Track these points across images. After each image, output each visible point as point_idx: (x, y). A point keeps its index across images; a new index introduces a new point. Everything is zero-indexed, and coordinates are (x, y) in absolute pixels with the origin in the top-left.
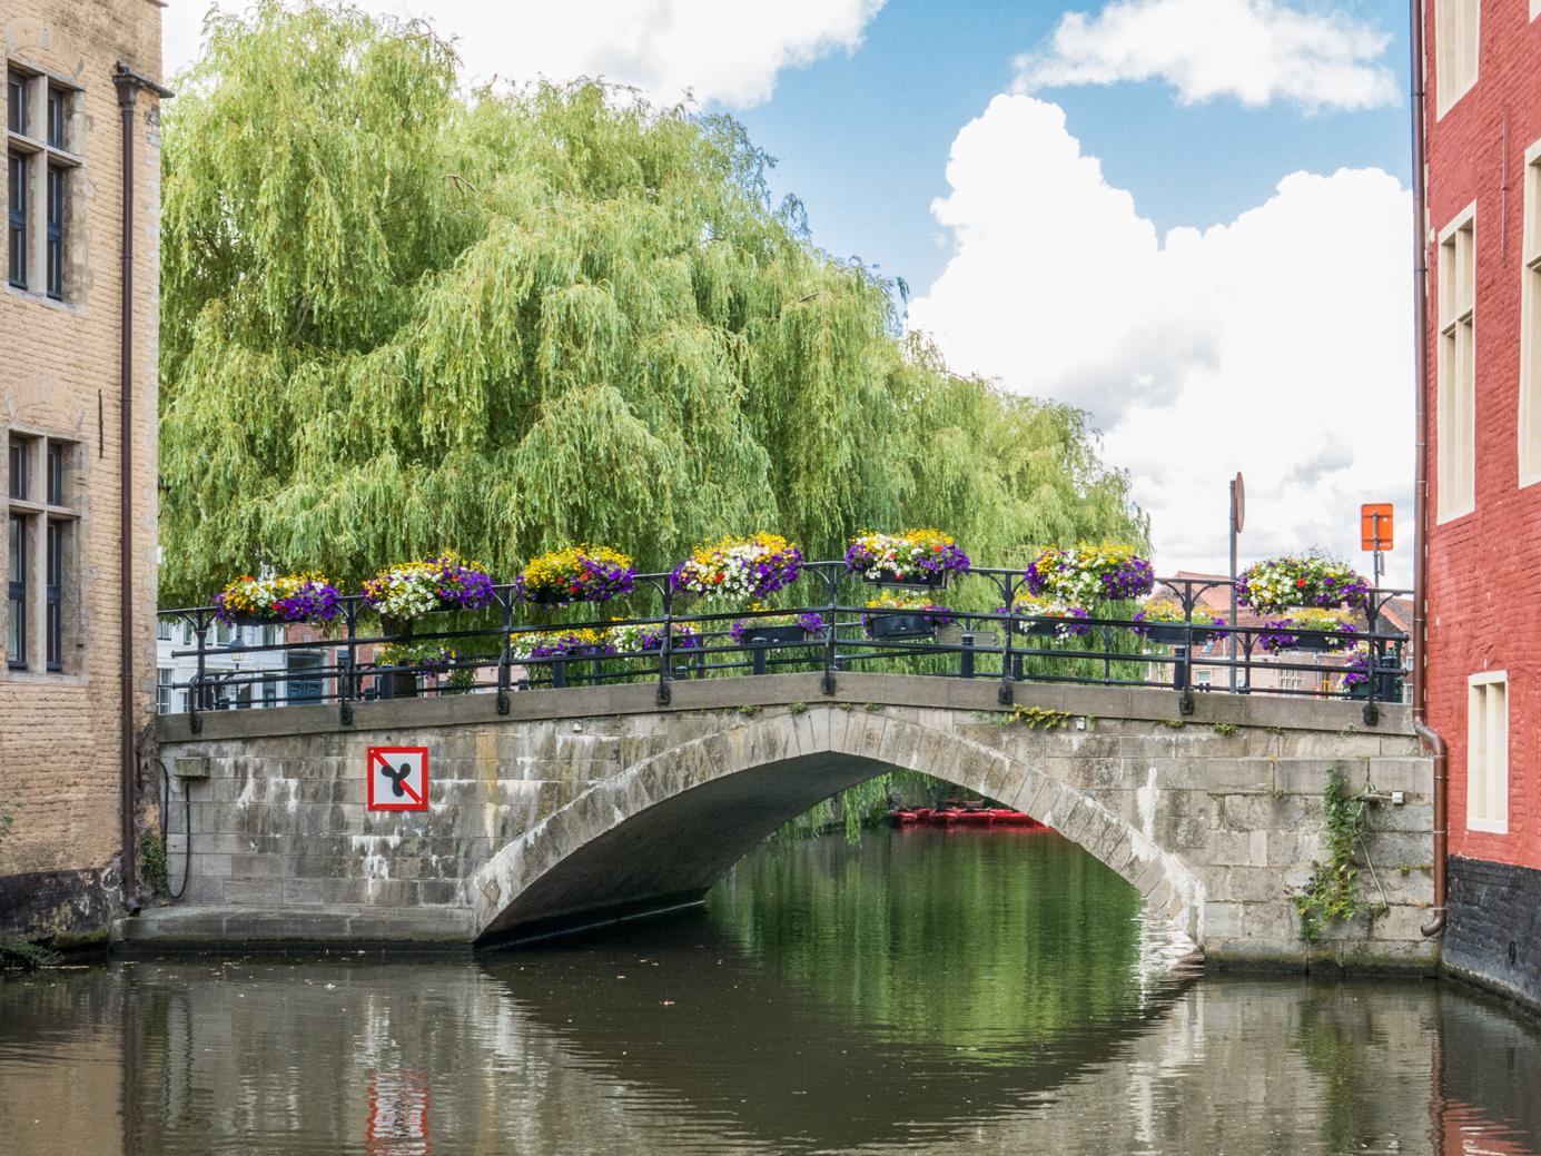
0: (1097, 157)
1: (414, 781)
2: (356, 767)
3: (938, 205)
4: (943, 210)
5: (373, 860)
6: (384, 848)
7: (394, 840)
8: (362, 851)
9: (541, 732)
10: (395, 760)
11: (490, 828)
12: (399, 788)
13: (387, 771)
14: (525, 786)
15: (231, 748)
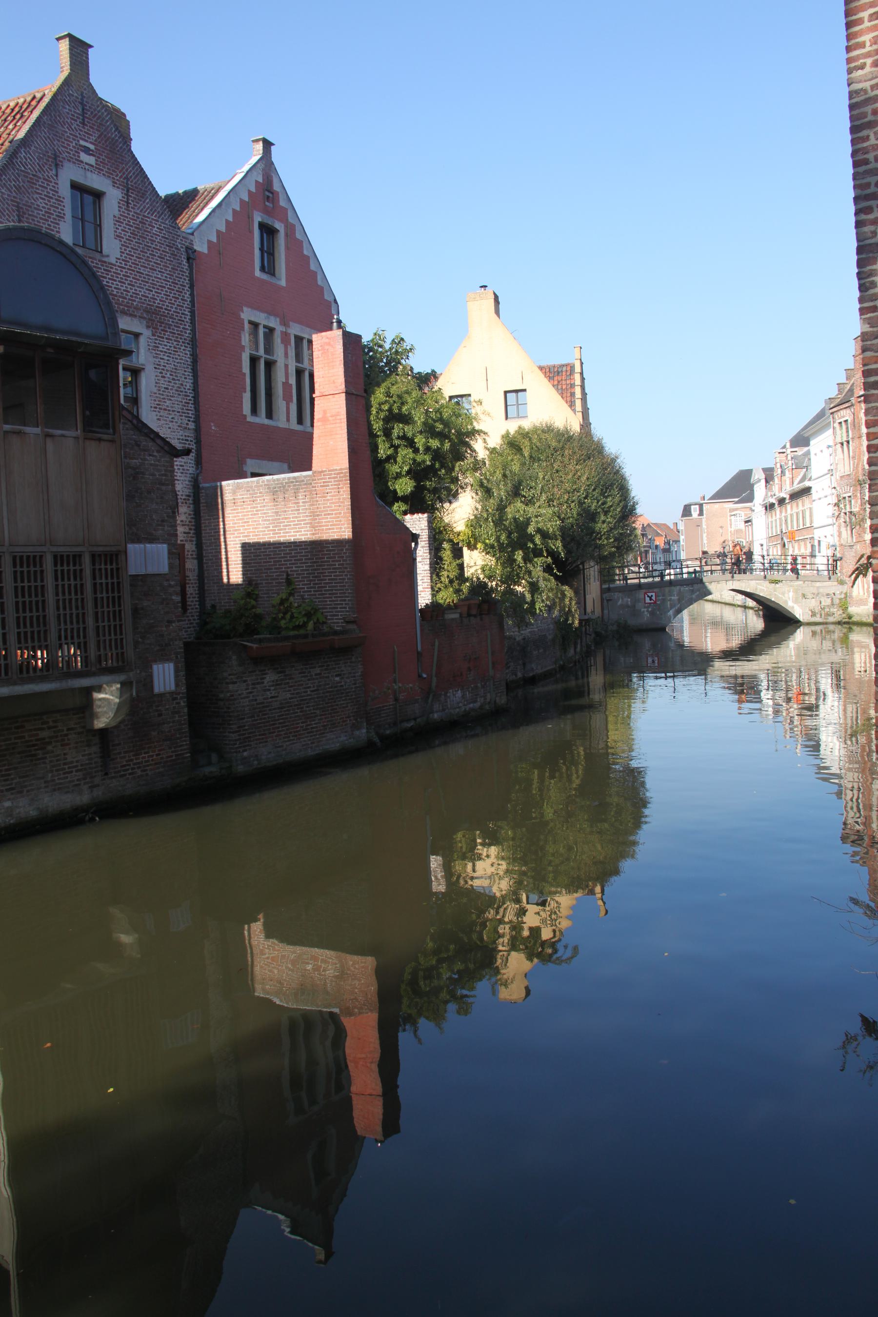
0: (244, 581)
1: (654, 598)
2: (642, 596)
3: (644, 810)
4: (365, 339)
5: (646, 613)
6: (648, 611)
7: (650, 609)
8: (644, 612)
9: (678, 587)
10: (650, 594)
11: (669, 606)
12: (651, 599)
13: (648, 596)
14: (675, 598)
15: (616, 594)
